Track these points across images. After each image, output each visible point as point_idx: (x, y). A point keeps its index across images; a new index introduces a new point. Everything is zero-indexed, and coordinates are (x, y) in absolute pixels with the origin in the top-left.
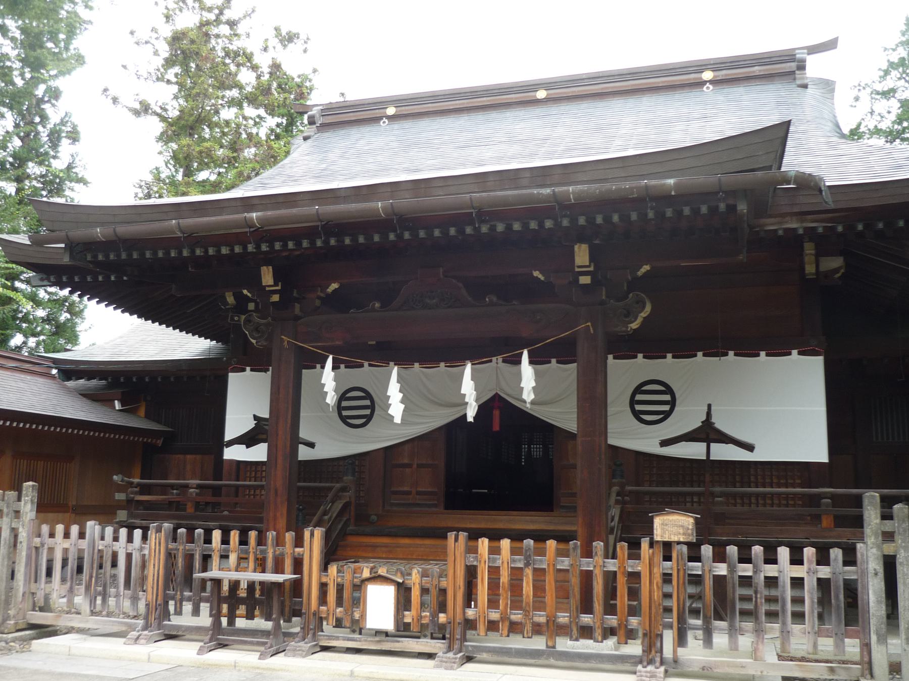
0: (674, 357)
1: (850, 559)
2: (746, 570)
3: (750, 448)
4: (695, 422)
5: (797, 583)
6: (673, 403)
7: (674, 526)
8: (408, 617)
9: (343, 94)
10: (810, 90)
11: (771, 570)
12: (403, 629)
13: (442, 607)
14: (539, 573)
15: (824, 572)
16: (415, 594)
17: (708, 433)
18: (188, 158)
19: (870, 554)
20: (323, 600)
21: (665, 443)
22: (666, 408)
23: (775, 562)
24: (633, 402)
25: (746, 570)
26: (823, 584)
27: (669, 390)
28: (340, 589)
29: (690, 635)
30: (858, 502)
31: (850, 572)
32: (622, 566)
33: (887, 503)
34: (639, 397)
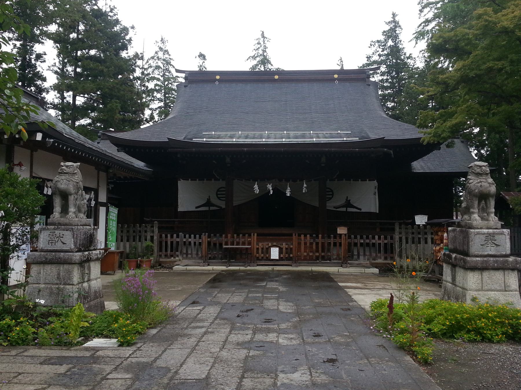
0: (338, 180)
1: (392, 238)
2: (368, 241)
3: (360, 209)
4: (343, 202)
5: (380, 244)
6: (333, 195)
7: (342, 231)
8: (282, 256)
9: (202, 56)
10: (371, 87)
11: (374, 241)
12: (281, 259)
13: (291, 253)
14: (317, 244)
15: (386, 242)
16: (284, 249)
17: (348, 204)
18: (22, 78)
19: (397, 237)
20: (258, 253)
21: (196, 208)
22: (331, 196)
23: (374, 239)
24: (217, 195)
25: (368, 241)
26: (386, 244)
27: (332, 191)
28: (262, 249)
29: (360, 257)
30: (394, 224)
31: (392, 241)
32: (370, 241)
33: (400, 224)
34: (219, 193)
